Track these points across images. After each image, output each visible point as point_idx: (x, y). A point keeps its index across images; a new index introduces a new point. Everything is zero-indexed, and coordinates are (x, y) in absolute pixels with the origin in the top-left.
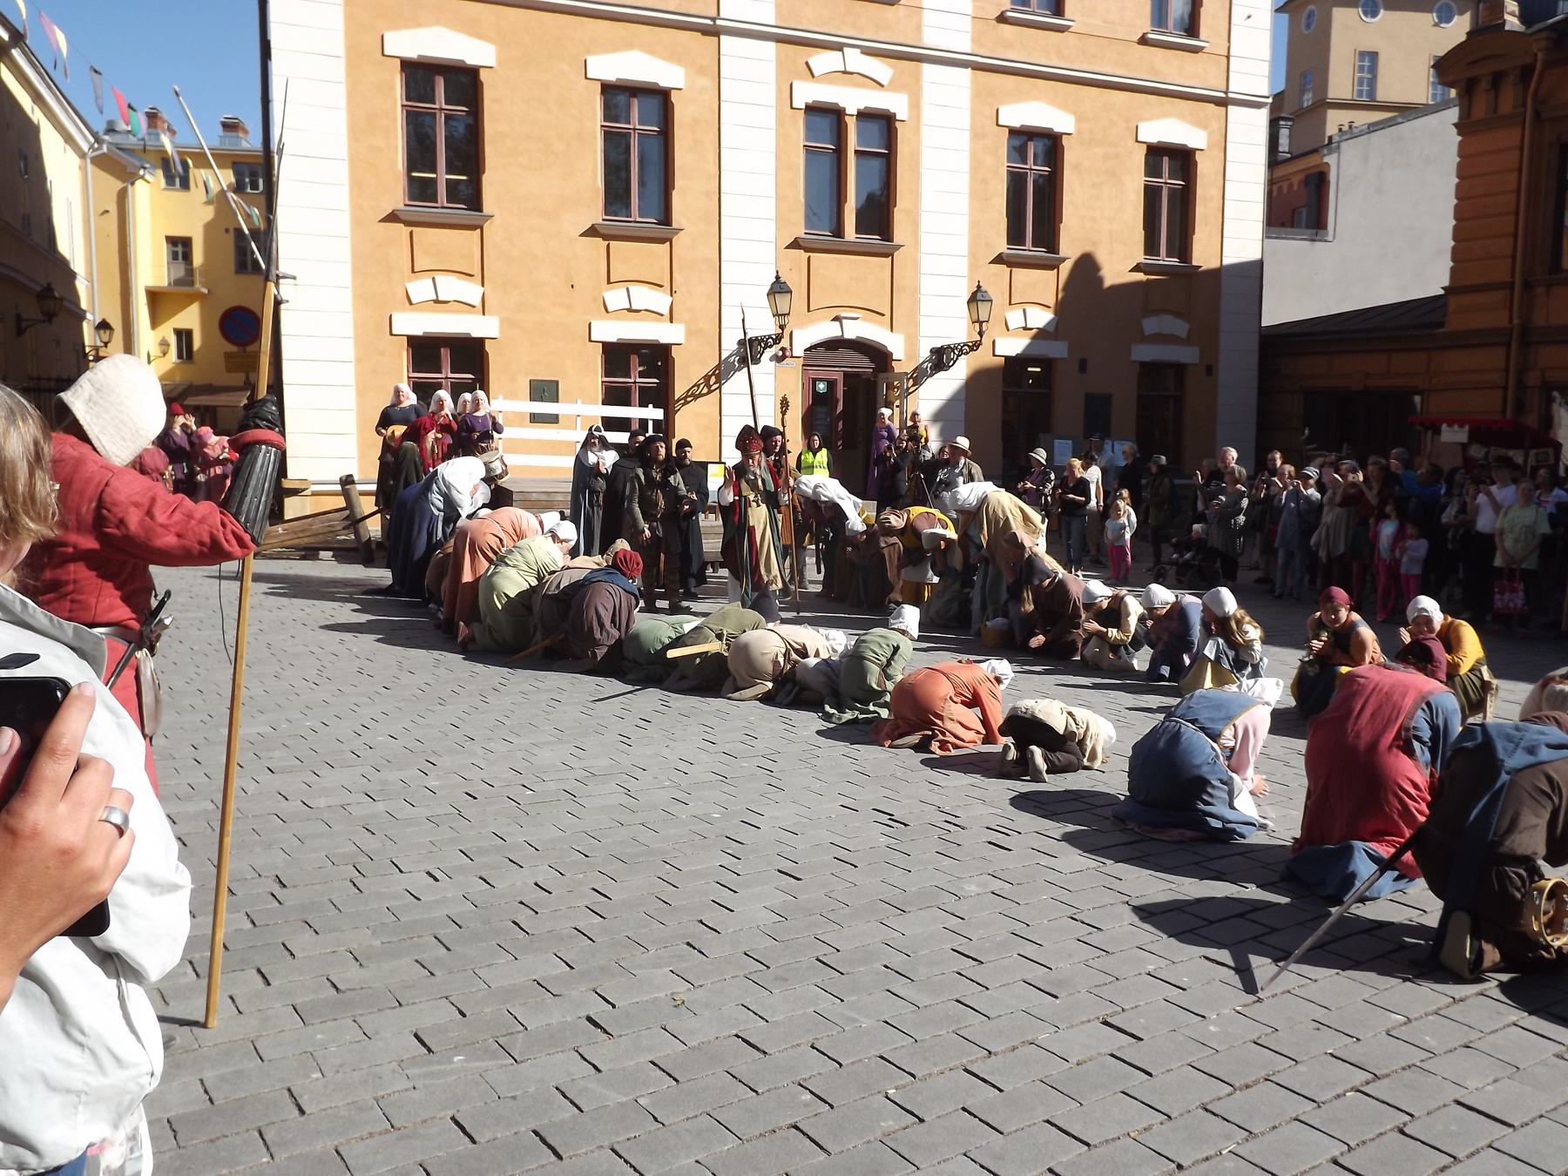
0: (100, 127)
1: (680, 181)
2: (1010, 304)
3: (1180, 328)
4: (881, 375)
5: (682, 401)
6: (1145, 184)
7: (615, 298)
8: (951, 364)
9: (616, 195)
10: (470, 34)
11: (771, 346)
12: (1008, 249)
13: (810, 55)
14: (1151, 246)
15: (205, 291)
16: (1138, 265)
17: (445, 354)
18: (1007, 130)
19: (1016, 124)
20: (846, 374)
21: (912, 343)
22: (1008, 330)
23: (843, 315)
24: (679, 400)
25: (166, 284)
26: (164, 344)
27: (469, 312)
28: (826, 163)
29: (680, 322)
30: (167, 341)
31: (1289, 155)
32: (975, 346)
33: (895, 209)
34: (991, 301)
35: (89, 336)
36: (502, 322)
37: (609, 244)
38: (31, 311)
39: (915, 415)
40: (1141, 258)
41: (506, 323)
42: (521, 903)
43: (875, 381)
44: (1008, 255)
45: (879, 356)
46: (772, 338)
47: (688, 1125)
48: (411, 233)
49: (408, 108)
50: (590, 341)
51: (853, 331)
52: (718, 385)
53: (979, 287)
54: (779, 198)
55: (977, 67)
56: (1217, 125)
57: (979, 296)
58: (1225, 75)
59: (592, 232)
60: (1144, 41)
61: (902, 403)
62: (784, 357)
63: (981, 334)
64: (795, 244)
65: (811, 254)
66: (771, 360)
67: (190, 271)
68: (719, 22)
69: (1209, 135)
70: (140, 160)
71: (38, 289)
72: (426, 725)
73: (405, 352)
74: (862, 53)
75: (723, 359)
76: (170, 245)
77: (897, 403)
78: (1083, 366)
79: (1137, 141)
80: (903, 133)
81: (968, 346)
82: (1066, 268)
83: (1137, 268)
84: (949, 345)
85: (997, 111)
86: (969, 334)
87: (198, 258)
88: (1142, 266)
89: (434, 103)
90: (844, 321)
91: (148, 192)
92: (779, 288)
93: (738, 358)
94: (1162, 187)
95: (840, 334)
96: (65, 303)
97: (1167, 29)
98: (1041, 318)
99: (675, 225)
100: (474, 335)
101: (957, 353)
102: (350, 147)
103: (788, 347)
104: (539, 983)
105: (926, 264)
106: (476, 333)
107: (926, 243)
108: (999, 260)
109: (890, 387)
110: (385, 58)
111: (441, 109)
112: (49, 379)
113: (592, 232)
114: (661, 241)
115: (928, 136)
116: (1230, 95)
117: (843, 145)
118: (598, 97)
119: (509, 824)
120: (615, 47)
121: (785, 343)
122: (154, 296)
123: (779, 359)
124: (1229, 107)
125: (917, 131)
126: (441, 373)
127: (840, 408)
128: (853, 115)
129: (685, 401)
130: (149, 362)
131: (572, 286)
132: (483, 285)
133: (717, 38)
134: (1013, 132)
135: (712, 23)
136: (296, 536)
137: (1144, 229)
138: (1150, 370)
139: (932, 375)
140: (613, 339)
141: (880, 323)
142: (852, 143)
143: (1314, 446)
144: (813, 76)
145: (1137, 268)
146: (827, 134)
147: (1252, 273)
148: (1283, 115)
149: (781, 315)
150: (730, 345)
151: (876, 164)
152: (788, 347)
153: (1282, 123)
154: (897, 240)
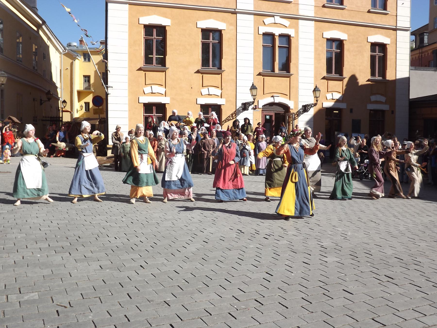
0: (65, 45)
1: (224, 56)
2: (328, 92)
3: (383, 99)
4: (287, 114)
5: (225, 122)
6: (370, 55)
7: (205, 91)
8: (308, 110)
9: (205, 62)
10: (163, 17)
11: (251, 105)
12: (327, 75)
13: (264, 19)
14: (373, 73)
15: (94, 91)
16: (324, 77)
17: (154, 108)
18: (326, 39)
19: (329, 37)
20: (276, 114)
21: (296, 104)
22: (327, 100)
23: (274, 95)
24: (223, 121)
25: (83, 89)
26: (82, 106)
27: (161, 96)
28: (269, 50)
29: (224, 98)
30: (82, 106)
31: (428, 44)
32: (315, 105)
33: (291, 63)
34: (320, 91)
35: (60, 105)
36: (171, 99)
37: (203, 76)
38: (44, 98)
39: (297, 126)
40: (370, 77)
41: (172, 99)
42: (135, 244)
43: (285, 115)
44: (327, 77)
45: (286, 108)
46: (251, 103)
47: (154, 284)
48: (264, 78)
49: (146, 38)
50: (197, 104)
51: (277, 100)
52: (235, 117)
53: (316, 87)
54: (255, 61)
55: (316, 21)
56: (393, 37)
57: (316, 90)
58: (396, 21)
59: (198, 72)
60: (369, 12)
61: (293, 122)
62: (256, 108)
63: (317, 101)
64: (260, 74)
65: (146, 72)
66: (252, 109)
67: (89, 85)
68: (236, 10)
69: (391, 40)
70: (77, 54)
71: (47, 91)
72: (128, 207)
73: (143, 108)
74: (280, 17)
75: (237, 109)
76: (84, 78)
77: (291, 122)
78: (351, 111)
79: (368, 42)
80: (293, 41)
81: (313, 104)
82: (346, 81)
83: (367, 81)
84: (308, 104)
85: (323, 33)
86: (314, 101)
87: (92, 81)
88: (370, 80)
89: (153, 37)
90: (275, 97)
91: (79, 62)
92: (253, 87)
93: (242, 108)
94: (376, 56)
95: (274, 101)
96: (53, 95)
97: (377, 8)
98: (337, 96)
99: (223, 69)
100: (163, 103)
101: (310, 107)
102: (129, 50)
103: (257, 105)
104: (132, 259)
105: (300, 79)
106: (219, 103)
107: (301, 73)
108: (324, 78)
109: (289, 117)
110: (139, 25)
111: (155, 38)
112: (48, 117)
113: (198, 72)
114: (219, 74)
115: (301, 42)
116: (397, 27)
117: (274, 44)
118: (200, 33)
119: (139, 229)
120: (205, 18)
121: (256, 104)
122: (79, 93)
123: (254, 109)
124: (397, 31)
125: (298, 40)
126: (153, 114)
127: (274, 124)
128: (277, 36)
129: (226, 121)
130: (77, 112)
131: (192, 88)
132: (165, 88)
133: (236, 15)
134: (328, 40)
135: (234, 10)
136: (108, 161)
137: (370, 69)
138: (376, 112)
139: (242, 112)
140: (204, 103)
141: (286, 98)
142: (277, 44)
143: (420, 136)
144: (265, 25)
145: (368, 80)
146: (270, 41)
147: (406, 81)
148: (425, 32)
149: (254, 96)
150: (239, 105)
151: (285, 50)
152: (257, 105)
153: (425, 34)
154: (291, 73)
